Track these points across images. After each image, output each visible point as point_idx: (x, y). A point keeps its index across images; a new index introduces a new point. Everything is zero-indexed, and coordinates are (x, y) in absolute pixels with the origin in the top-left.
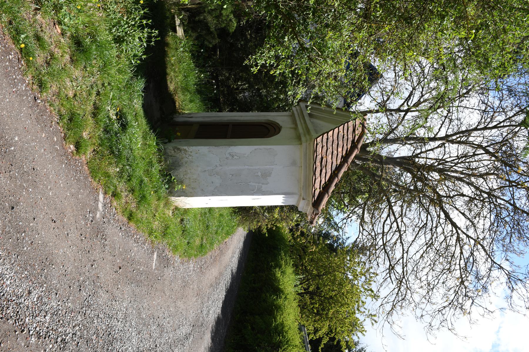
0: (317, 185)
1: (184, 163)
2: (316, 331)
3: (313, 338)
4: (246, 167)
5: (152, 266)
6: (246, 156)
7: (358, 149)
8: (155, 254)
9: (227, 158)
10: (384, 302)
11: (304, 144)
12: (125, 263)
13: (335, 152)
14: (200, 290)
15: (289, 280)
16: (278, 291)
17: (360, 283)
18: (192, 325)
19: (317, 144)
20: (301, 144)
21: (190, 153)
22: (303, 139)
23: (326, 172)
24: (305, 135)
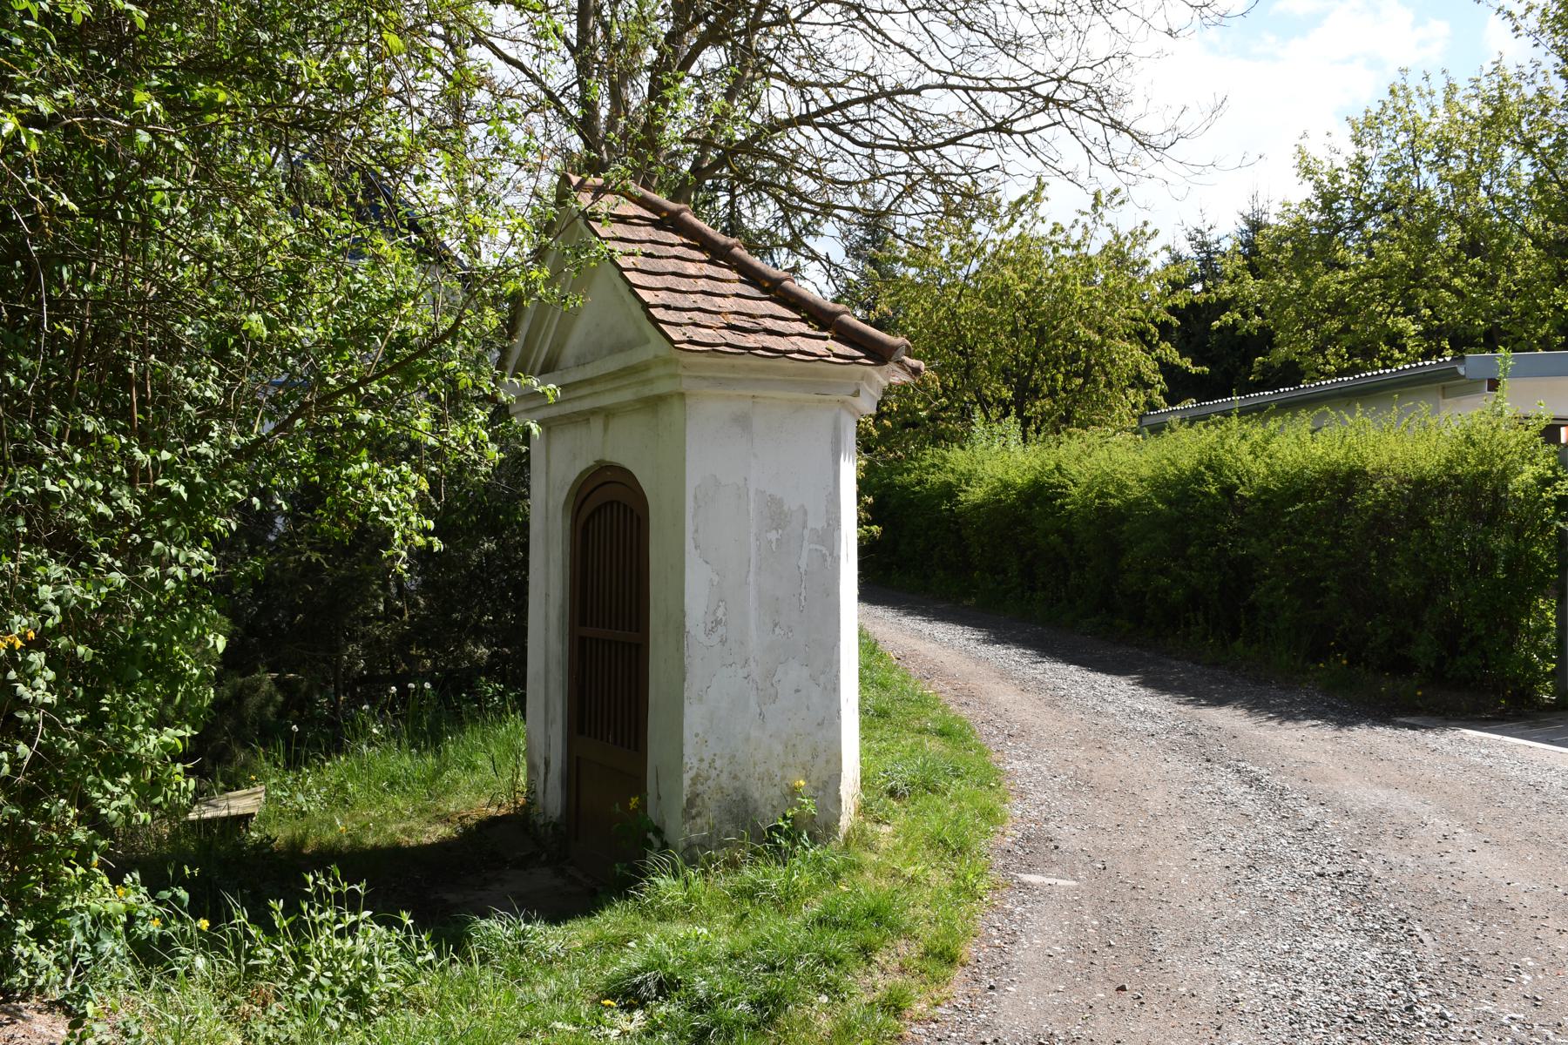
0: (818, 347)
1: (737, 784)
2: (1139, 382)
3: (1162, 393)
4: (751, 578)
5: (1068, 889)
6: (716, 579)
7: (681, 211)
8: (1026, 878)
9: (723, 642)
10: (1105, 158)
11: (685, 385)
12: (1097, 972)
13: (703, 284)
14: (1083, 740)
15: (994, 459)
16: (1039, 495)
17: (993, 236)
18: (1209, 765)
19: (691, 342)
20: (682, 395)
21: (705, 765)
22: (662, 387)
23: (772, 316)
24: (651, 381)
